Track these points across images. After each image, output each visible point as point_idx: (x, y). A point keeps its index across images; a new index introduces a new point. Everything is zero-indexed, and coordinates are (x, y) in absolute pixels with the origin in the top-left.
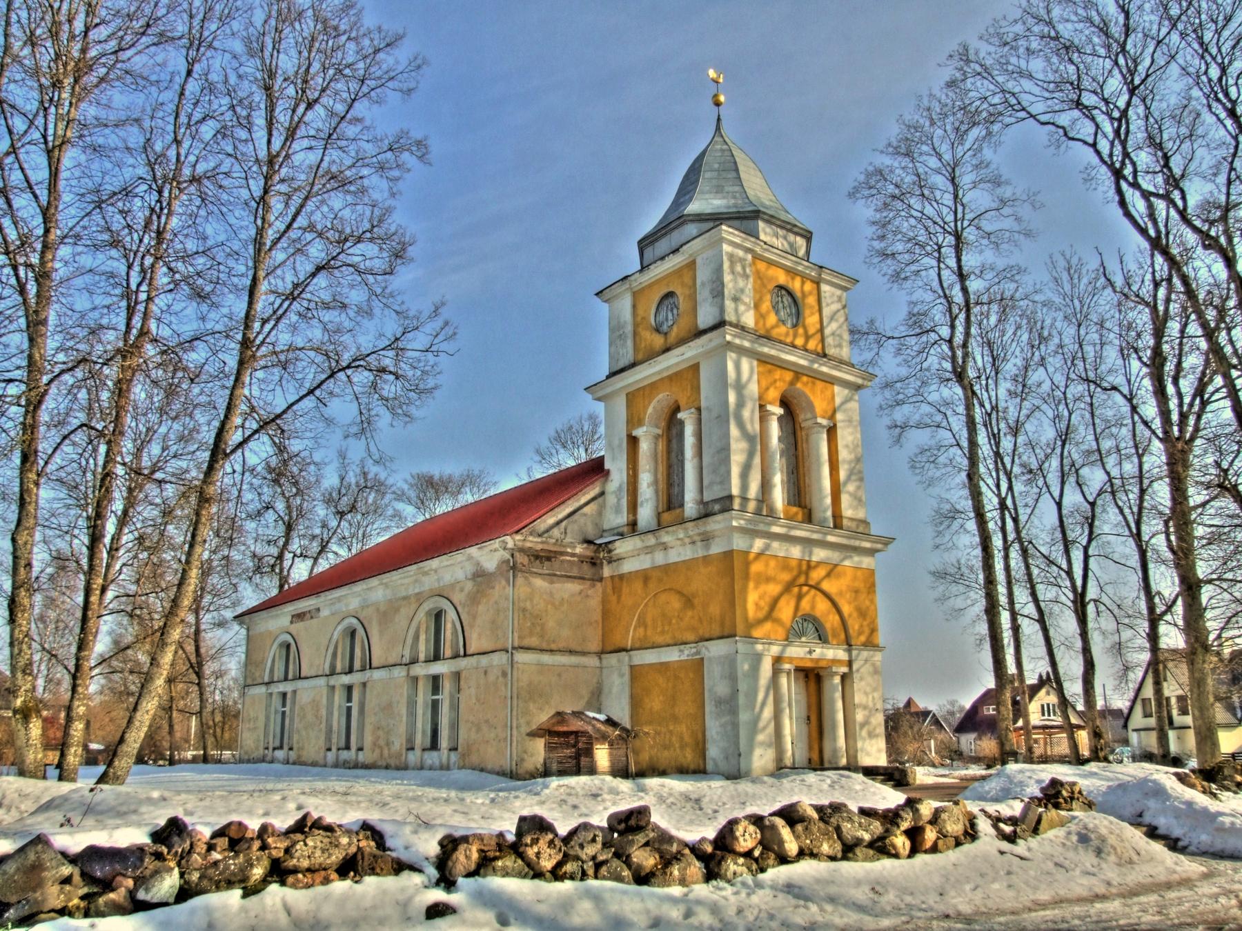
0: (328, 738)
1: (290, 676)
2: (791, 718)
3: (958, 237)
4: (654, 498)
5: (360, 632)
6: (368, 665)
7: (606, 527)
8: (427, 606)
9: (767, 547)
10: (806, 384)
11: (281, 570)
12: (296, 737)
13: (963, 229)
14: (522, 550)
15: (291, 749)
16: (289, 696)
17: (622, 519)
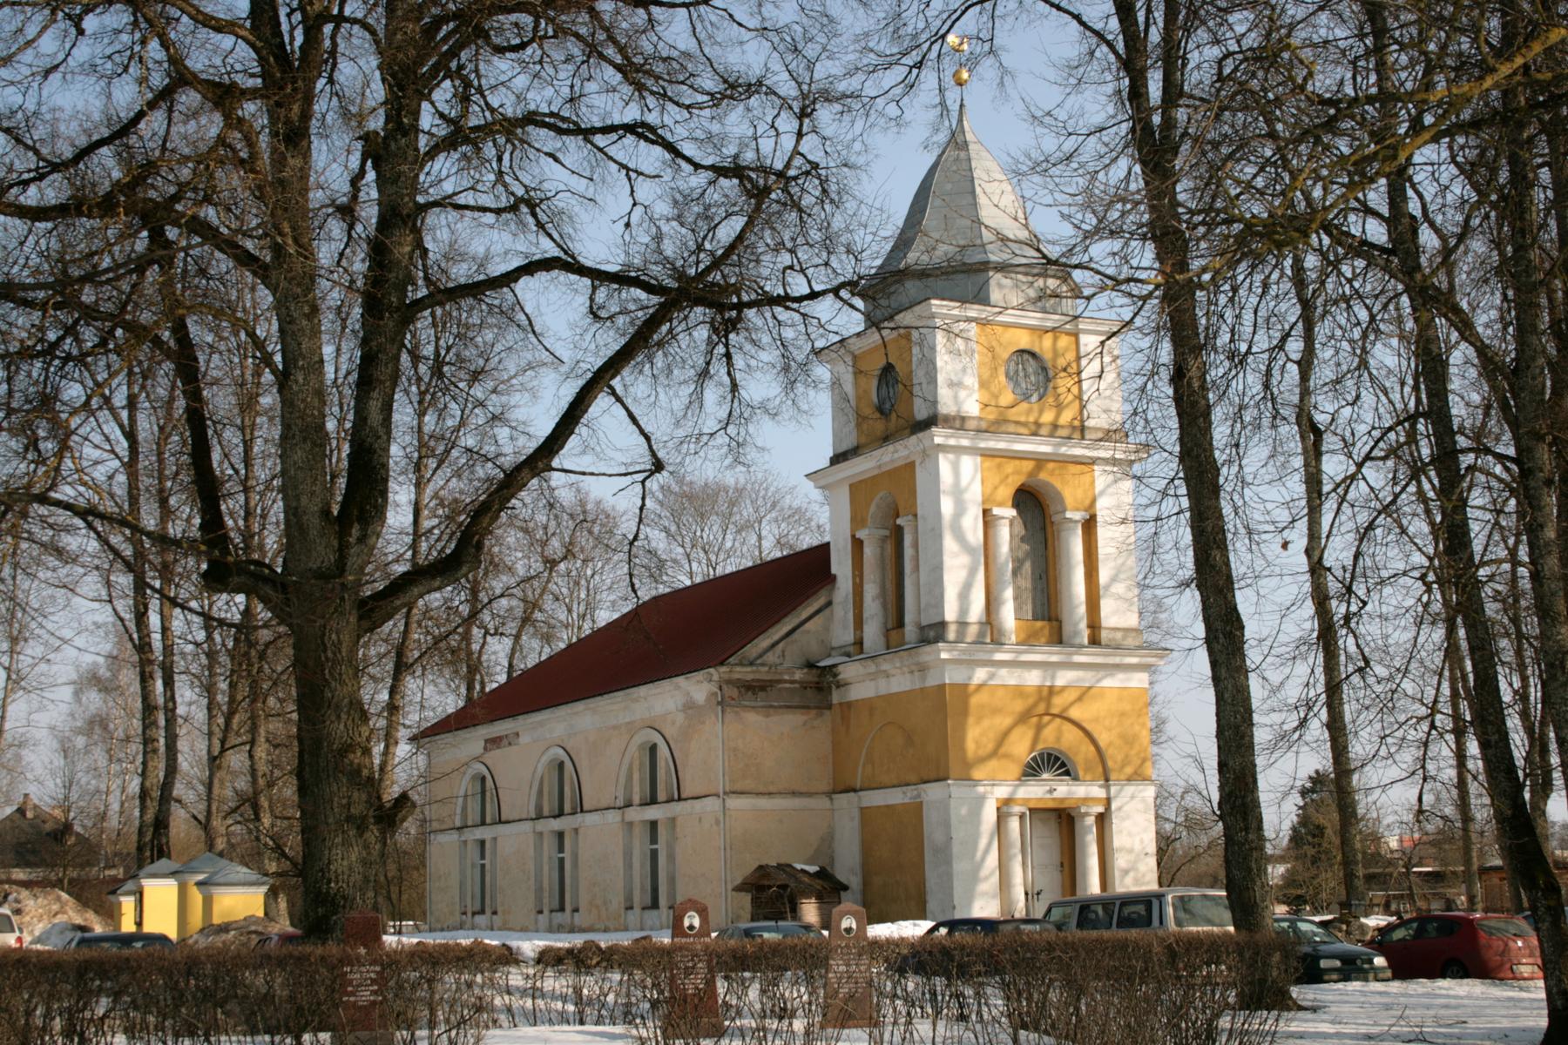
0: (539, 899)
1: (488, 820)
2: (1024, 864)
5: (568, 764)
7: (835, 644)
8: (639, 739)
9: (992, 676)
10: (1052, 473)
12: (499, 898)
14: (729, 682)
15: (495, 913)
16: (488, 845)
17: (848, 637)
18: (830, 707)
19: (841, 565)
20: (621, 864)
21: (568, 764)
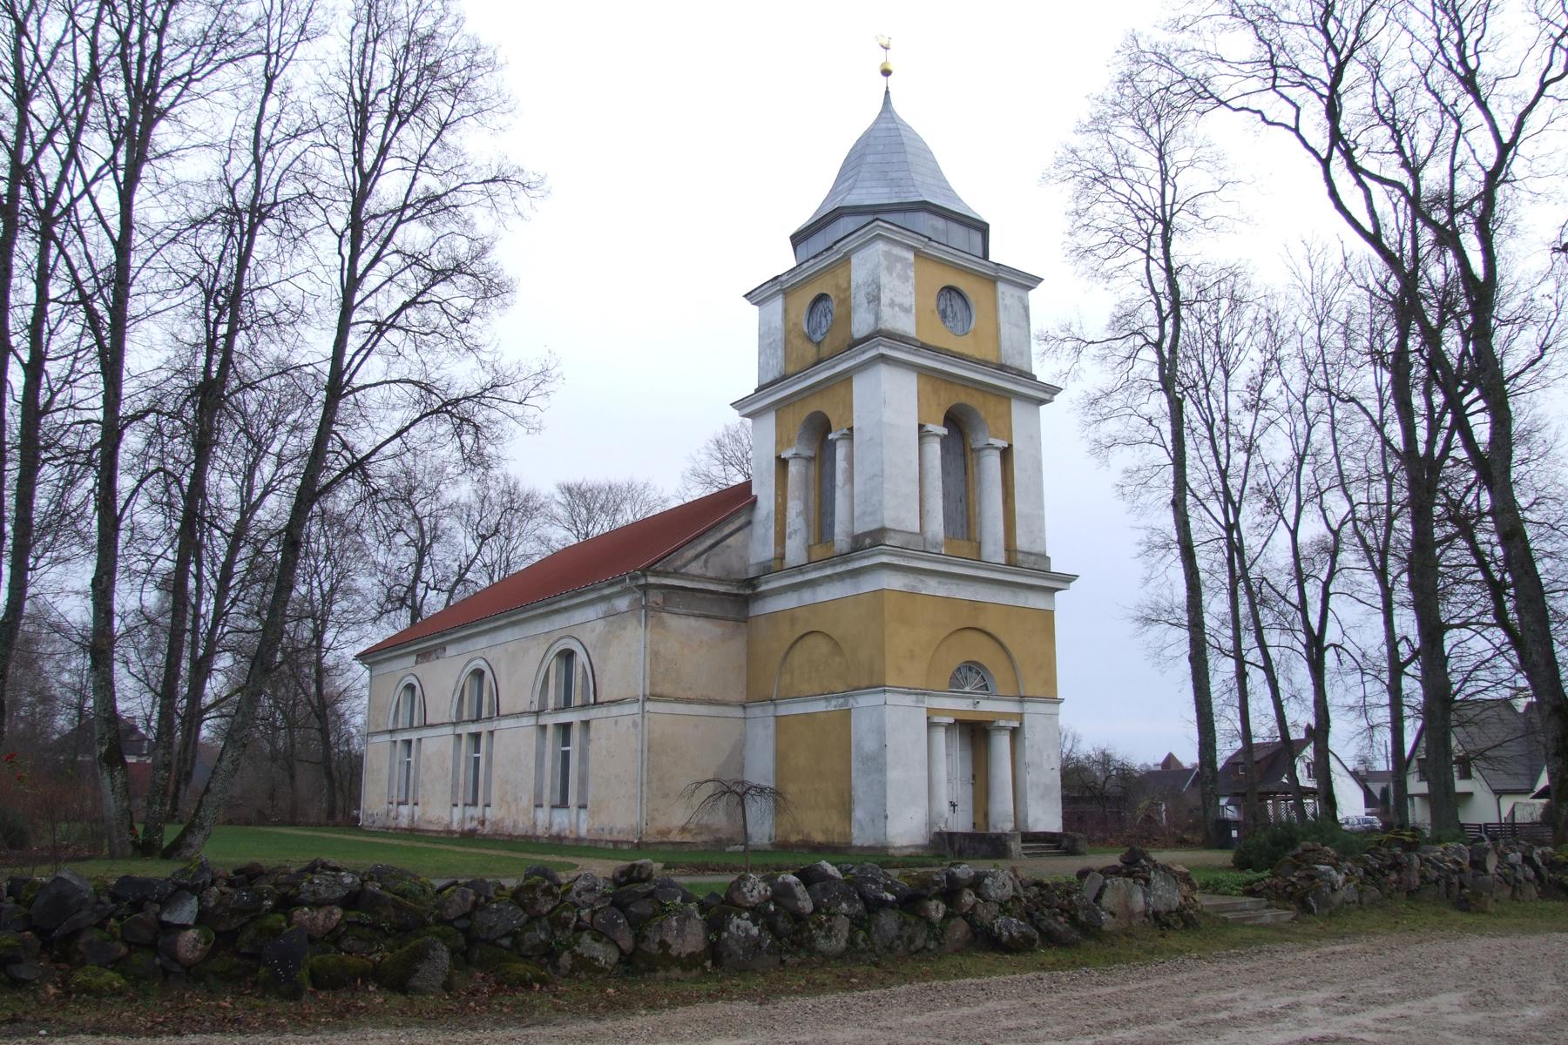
0: (454, 793)
3: (1167, 225)
4: (804, 530)
6: (495, 714)
11: (414, 601)
13: (1172, 215)
15: (583, 807)
18: (746, 620)
19: (765, 493)
20: (532, 764)
21: (488, 674)
